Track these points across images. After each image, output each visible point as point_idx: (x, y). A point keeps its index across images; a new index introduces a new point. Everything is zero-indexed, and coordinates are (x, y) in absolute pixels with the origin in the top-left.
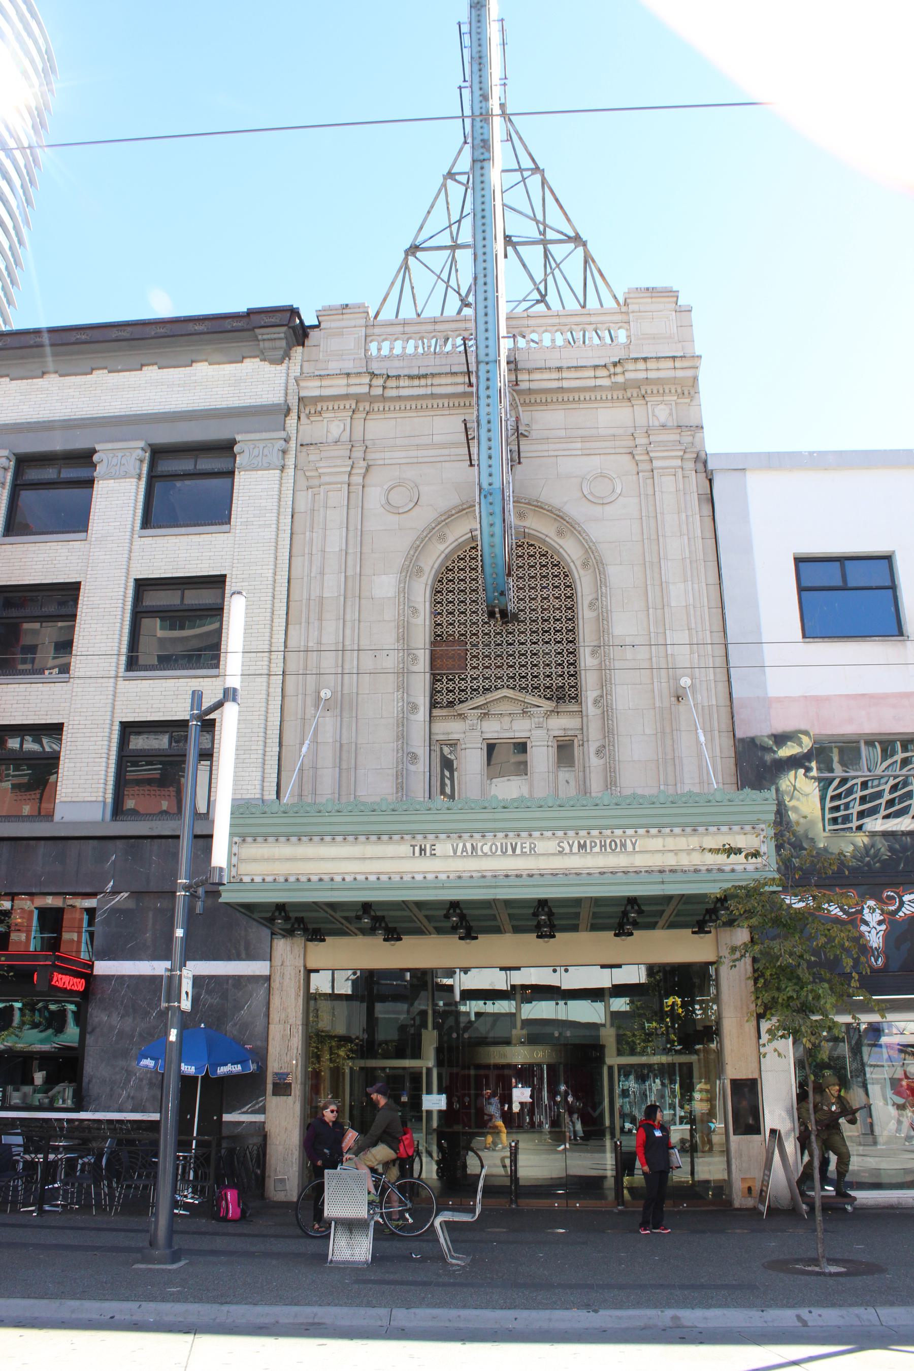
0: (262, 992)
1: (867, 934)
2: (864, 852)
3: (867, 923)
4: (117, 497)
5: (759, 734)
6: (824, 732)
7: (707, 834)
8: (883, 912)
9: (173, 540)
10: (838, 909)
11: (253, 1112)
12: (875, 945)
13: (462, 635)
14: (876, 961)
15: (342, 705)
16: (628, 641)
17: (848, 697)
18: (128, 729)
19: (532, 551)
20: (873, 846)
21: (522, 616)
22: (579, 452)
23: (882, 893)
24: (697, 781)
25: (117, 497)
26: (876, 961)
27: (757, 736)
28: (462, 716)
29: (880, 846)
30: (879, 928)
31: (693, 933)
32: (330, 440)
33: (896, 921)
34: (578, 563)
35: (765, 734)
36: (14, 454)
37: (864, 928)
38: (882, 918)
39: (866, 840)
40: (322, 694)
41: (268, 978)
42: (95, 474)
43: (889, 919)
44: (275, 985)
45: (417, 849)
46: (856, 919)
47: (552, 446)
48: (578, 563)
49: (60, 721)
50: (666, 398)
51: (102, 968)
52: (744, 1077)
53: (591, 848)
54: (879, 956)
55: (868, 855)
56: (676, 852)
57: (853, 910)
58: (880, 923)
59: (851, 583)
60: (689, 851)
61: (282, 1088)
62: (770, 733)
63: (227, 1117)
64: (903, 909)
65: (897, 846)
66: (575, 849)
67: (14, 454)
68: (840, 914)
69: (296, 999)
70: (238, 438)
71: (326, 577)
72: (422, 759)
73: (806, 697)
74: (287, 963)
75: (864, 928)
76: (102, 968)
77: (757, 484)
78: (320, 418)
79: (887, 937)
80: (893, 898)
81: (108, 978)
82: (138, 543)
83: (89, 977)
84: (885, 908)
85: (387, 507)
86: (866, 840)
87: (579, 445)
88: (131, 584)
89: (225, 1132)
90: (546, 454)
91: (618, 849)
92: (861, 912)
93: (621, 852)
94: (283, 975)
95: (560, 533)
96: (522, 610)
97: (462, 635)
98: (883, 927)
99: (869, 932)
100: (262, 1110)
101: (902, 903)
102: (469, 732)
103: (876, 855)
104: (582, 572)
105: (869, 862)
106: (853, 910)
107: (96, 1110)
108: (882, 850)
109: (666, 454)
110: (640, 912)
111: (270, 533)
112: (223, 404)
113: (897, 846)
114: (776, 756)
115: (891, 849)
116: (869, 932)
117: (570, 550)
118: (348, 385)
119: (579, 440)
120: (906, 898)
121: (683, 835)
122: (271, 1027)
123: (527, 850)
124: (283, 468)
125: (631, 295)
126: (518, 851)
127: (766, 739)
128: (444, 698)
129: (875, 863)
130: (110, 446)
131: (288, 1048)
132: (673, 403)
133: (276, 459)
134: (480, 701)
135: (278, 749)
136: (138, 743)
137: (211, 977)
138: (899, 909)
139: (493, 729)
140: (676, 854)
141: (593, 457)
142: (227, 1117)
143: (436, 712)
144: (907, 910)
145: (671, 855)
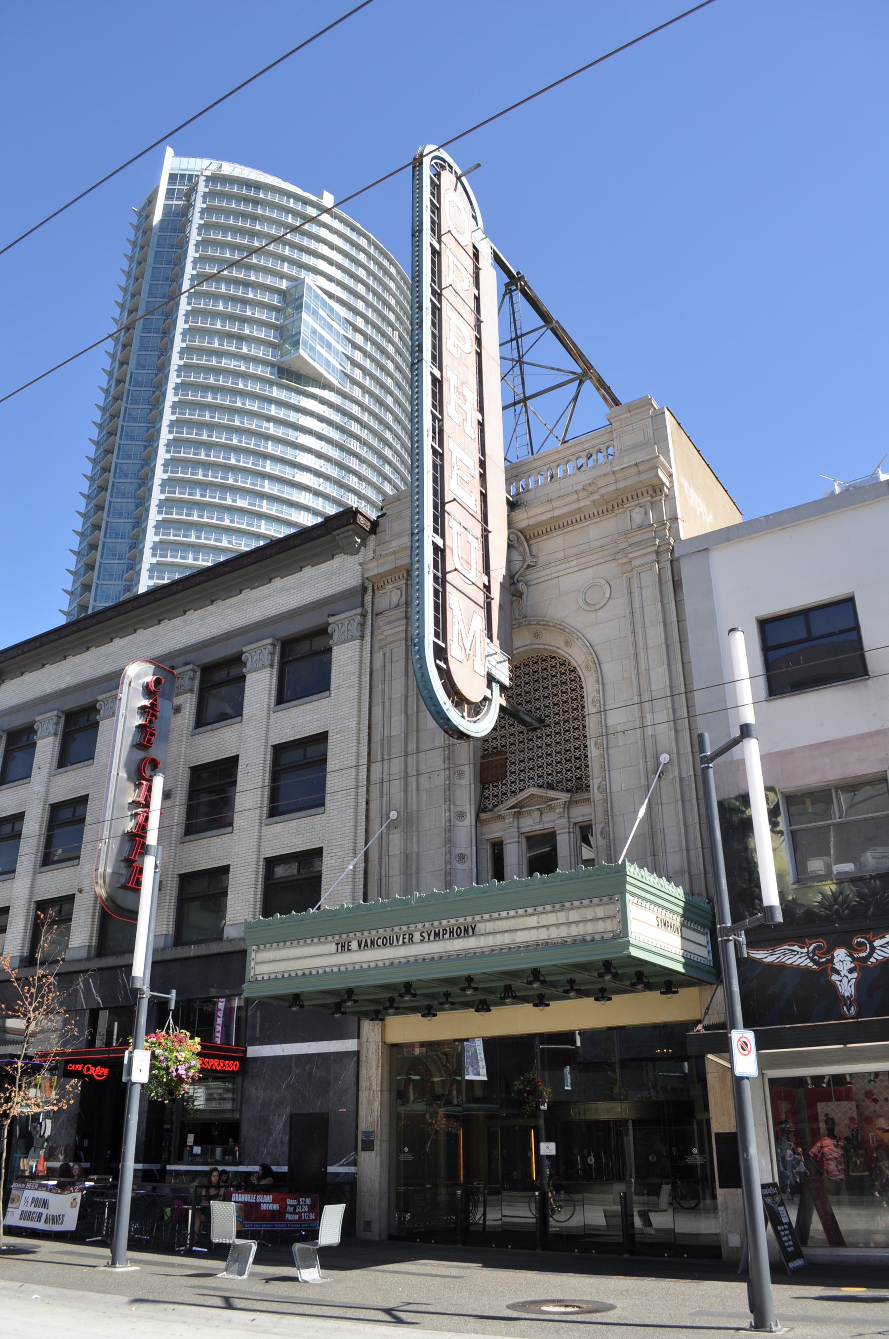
0: (352, 1065)
1: (838, 983)
2: (831, 899)
3: (838, 972)
4: (259, 685)
5: (726, 797)
6: (847, 775)
7: (572, 909)
8: (854, 960)
9: (294, 710)
10: (808, 960)
11: (347, 1165)
12: (847, 994)
13: (503, 746)
14: (849, 1010)
15: (408, 822)
16: (620, 728)
17: (811, 747)
18: (271, 863)
19: (553, 662)
20: (841, 893)
21: (548, 721)
22: (576, 569)
23: (852, 940)
24: (677, 849)
25: (259, 685)
26: (849, 1010)
27: (724, 800)
28: (501, 818)
29: (848, 892)
30: (850, 976)
31: (662, 993)
32: (393, 606)
33: (868, 967)
34: (583, 667)
35: (733, 796)
36: (63, 712)
37: (835, 977)
38: (853, 965)
39: (834, 887)
40: (391, 815)
41: (358, 1053)
42: (244, 670)
43: (860, 965)
44: (363, 1058)
45: (340, 946)
46: (828, 968)
47: (554, 569)
48: (583, 667)
49: (225, 864)
50: (641, 501)
51: (254, 1051)
52: (728, 1131)
53: (444, 934)
54: (851, 1005)
55: (836, 903)
56: (547, 927)
57: (824, 960)
58: (851, 971)
59: (816, 633)
60: (558, 925)
61: (368, 1146)
62: (737, 794)
63: (331, 1169)
64: (875, 955)
65: (866, 891)
66: (432, 937)
67: (63, 712)
68: (811, 964)
69: (377, 1069)
70: (244, 649)
71: (393, 719)
72: (469, 858)
73: (771, 754)
74: (371, 1040)
75: (835, 977)
76: (254, 1051)
77: (721, 560)
78: (623, 510)
79: (858, 984)
80: (864, 944)
81: (255, 1059)
82: (273, 716)
83: (244, 1060)
84: (856, 956)
85: (585, 607)
86: (834, 887)
87: (575, 563)
88: (269, 750)
89: (329, 1180)
90: (550, 577)
91: (388, 944)
92: (831, 961)
93: (464, 937)
94: (368, 1049)
95: (567, 643)
96: (548, 716)
97: (503, 746)
98: (855, 975)
99: (841, 981)
100: (355, 1163)
101: (873, 949)
102: (510, 831)
103: (845, 901)
104: (586, 673)
105: (837, 910)
106: (824, 960)
107: (248, 1164)
108: (851, 896)
109: (641, 552)
110: (616, 976)
111: (354, 692)
112: (322, 595)
113: (866, 891)
114: (745, 816)
115: (860, 894)
116: (841, 981)
117: (577, 656)
118: (639, 473)
119: (575, 558)
120: (877, 943)
121: (553, 912)
122: (360, 1093)
123: (406, 940)
124: (362, 637)
125: (613, 415)
126: (401, 942)
127: (734, 801)
128: (489, 804)
129: (843, 911)
130: (104, 696)
131: (372, 1111)
132: (648, 504)
133: (355, 631)
134: (512, 801)
135: (363, 865)
136: (280, 871)
137: (319, 1055)
138: (870, 955)
139: (532, 823)
140: (548, 929)
141: (587, 570)
142: (331, 1169)
143: (483, 816)
144: (878, 956)
145: (544, 929)
